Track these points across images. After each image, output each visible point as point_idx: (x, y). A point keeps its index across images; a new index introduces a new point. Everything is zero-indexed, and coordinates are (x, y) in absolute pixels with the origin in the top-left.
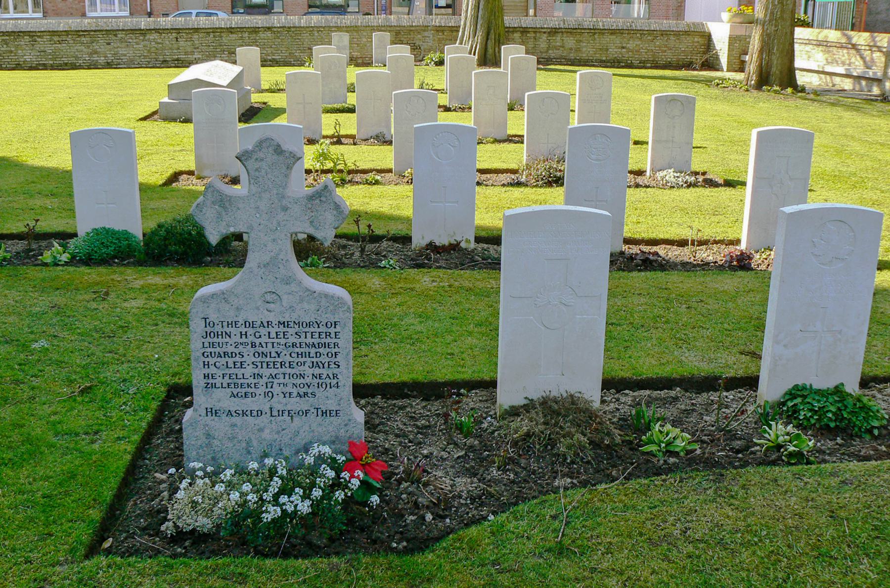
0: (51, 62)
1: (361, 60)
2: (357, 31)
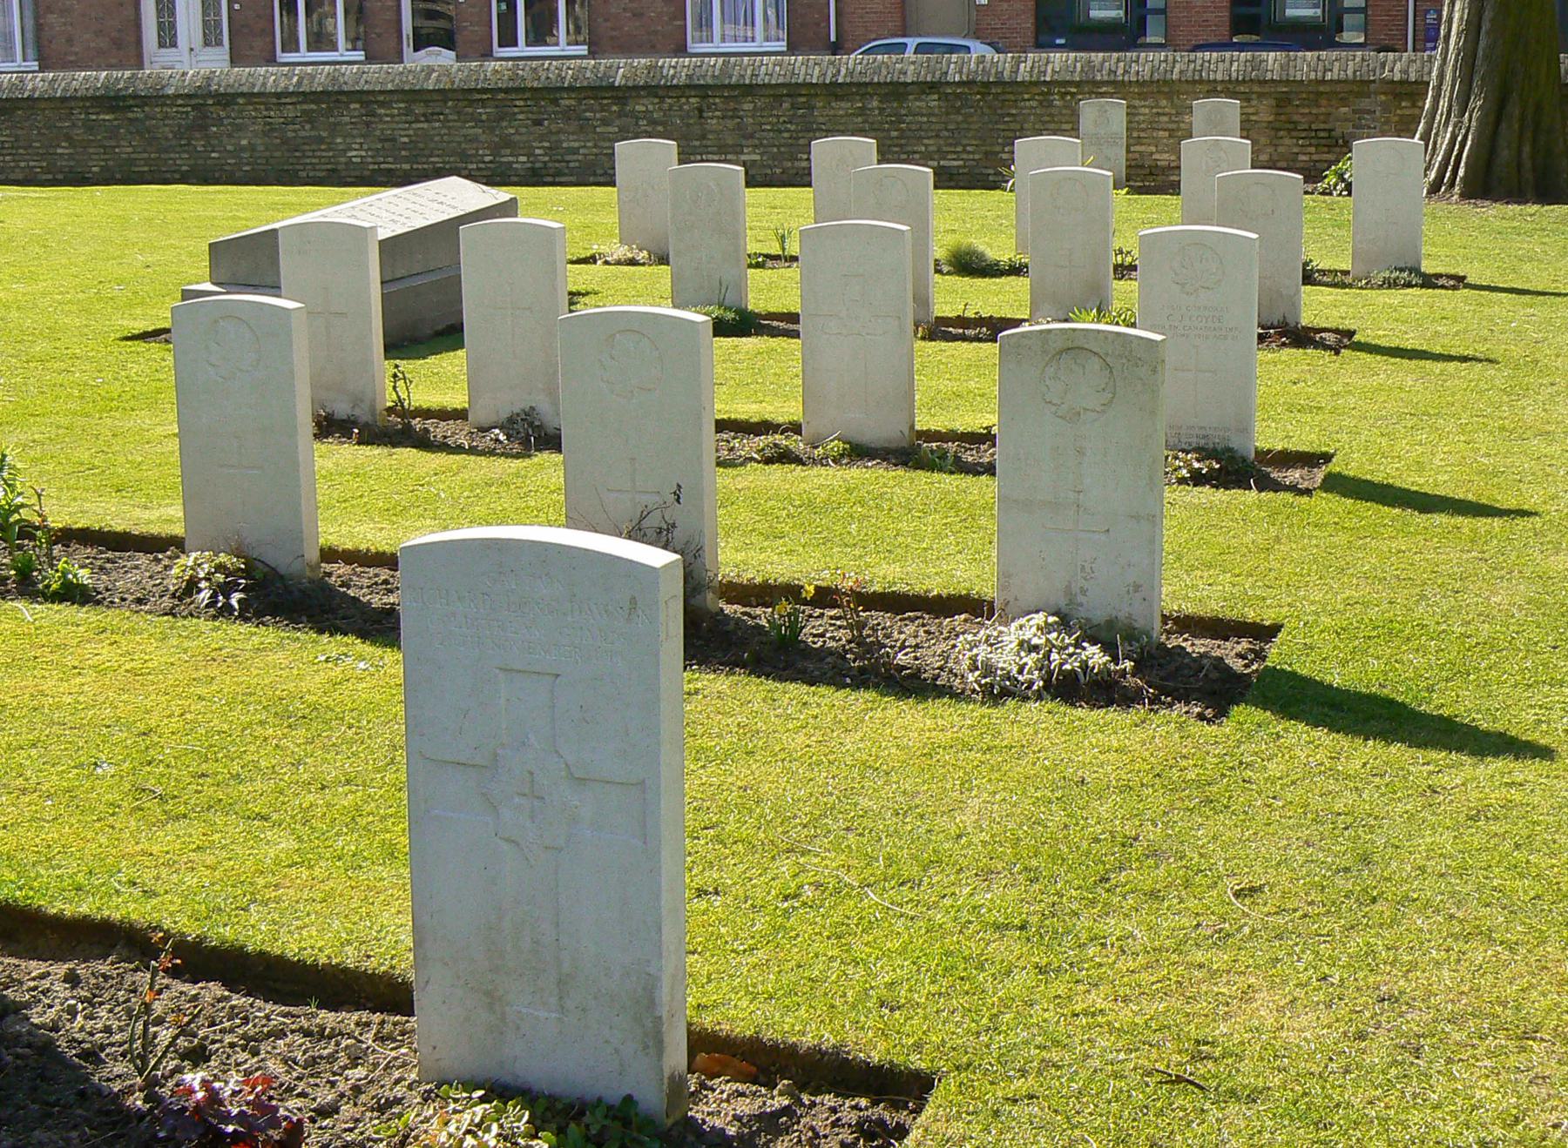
0: (406, 166)
1: (1150, 176)
2: (1169, 96)
